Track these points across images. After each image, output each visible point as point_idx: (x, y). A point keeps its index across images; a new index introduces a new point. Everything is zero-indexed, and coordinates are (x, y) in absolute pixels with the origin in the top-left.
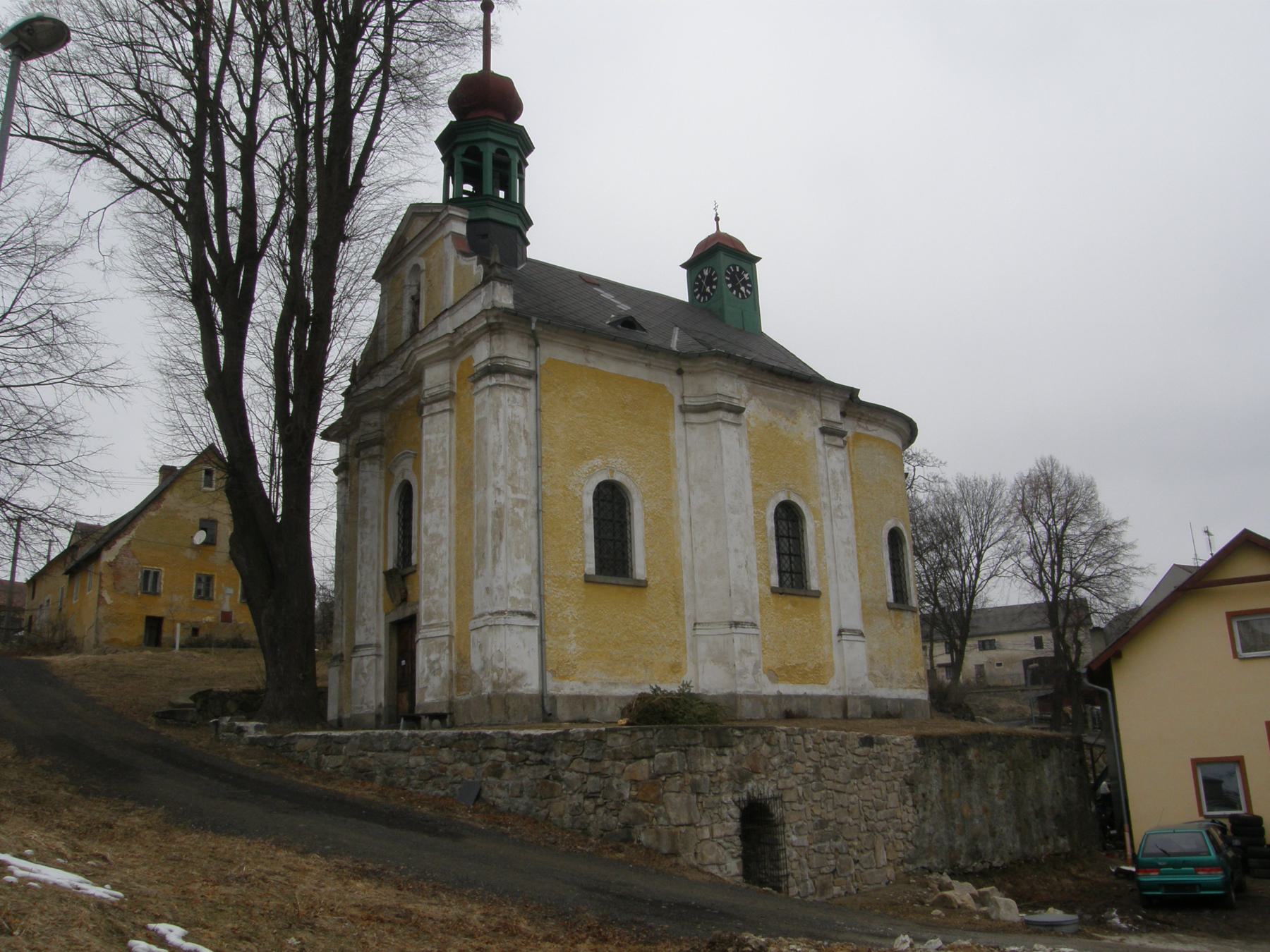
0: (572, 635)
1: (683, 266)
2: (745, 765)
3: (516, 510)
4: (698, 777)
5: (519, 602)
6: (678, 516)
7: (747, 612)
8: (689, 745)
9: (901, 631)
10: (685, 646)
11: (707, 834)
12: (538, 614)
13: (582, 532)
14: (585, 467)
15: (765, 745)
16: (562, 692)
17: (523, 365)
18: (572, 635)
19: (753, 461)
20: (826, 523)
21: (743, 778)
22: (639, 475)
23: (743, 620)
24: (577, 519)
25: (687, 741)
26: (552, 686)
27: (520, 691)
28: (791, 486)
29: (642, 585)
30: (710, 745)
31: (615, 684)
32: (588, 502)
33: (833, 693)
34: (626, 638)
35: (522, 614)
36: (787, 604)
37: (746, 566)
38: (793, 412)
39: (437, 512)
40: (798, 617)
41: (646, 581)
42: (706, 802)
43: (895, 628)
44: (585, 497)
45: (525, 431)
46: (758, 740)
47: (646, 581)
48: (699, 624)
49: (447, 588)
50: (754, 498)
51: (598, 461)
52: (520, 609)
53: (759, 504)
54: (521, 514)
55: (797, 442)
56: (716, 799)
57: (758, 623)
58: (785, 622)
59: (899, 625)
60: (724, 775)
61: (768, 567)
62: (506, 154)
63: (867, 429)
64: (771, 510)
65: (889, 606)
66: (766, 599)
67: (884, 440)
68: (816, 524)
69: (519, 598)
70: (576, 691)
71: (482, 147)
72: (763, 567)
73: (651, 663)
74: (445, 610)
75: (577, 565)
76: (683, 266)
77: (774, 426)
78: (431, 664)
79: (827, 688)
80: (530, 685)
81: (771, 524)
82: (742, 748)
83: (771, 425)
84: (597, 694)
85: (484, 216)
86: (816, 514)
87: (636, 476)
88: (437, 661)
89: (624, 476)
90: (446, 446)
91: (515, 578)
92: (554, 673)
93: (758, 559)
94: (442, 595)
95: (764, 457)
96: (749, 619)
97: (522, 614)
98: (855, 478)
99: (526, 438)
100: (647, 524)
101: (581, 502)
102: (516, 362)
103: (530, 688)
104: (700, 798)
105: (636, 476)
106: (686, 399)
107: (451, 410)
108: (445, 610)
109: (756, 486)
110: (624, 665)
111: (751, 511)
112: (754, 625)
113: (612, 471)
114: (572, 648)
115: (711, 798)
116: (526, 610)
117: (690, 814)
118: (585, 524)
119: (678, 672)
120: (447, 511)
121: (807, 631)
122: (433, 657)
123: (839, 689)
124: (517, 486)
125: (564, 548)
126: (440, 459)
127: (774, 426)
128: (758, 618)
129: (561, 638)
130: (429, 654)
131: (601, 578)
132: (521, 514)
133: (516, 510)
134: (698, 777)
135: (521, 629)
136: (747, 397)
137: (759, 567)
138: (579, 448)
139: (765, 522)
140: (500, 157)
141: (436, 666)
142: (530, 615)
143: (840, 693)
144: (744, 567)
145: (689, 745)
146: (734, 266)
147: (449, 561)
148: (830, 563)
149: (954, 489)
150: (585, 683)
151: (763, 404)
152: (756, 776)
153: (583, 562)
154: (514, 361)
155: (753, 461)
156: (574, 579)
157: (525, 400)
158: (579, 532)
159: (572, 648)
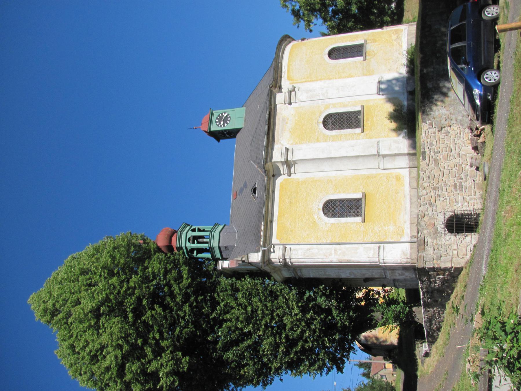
0: (386, 228)
2: (431, 231)
3: (338, 254)
4: (435, 257)
8: (424, 260)
9: (375, 52)
10: (388, 173)
11: (455, 252)
12: (378, 245)
13: (345, 223)
15: (424, 219)
16: (409, 233)
18: (386, 228)
20: (330, 101)
21: (436, 232)
22: (319, 196)
26: (407, 238)
27: (409, 253)
29: (364, 195)
32: (333, 220)
33: (406, 97)
35: (379, 252)
36: (367, 124)
41: (363, 193)
42: (444, 252)
43: (375, 56)
44: (331, 222)
46: (422, 223)
48: (378, 152)
49: (371, 271)
51: (315, 216)
53: (326, 139)
54: (340, 252)
56: (443, 247)
57: (377, 140)
59: (373, 53)
60: (435, 242)
64: (328, 132)
69: (373, 253)
71: (189, 249)
72: (353, 136)
73: (396, 190)
74: (379, 271)
76: (219, 141)
77: (291, 130)
78: (400, 275)
79: (404, 101)
80: (406, 248)
83: (290, 132)
84: (410, 217)
85: (218, 248)
86: (327, 107)
88: (399, 274)
91: (365, 254)
93: (349, 139)
96: (376, 145)
98: (308, 80)
100: (339, 192)
101: (333, 224)
103: (408, 248)
106: (285, 173)
107: (301, 270)
108: (379, 271)
109: (318, 141)
110: (397, 204)
112: (378, 143)
113: (319, 209)
114: (391, 228)
115: (443, 250)
116: (377, 250)
117: (448, 262)
118: (342, 222)
121: (379, 113)
122: (398, 275)
123: (404, 94)
126: (320, 273)
127: (291, 130)
128: (375, 140)
132: (340, 252)
135: (385, 252)
138: (311, 224)
142: (379, 248)
143: (406, 94)
145: (424, 260)
146: (216, 122)
148: (348, 99)
150: (405, 222)
153: (357, 223)
156: (364, 227)
157: (295, 250)
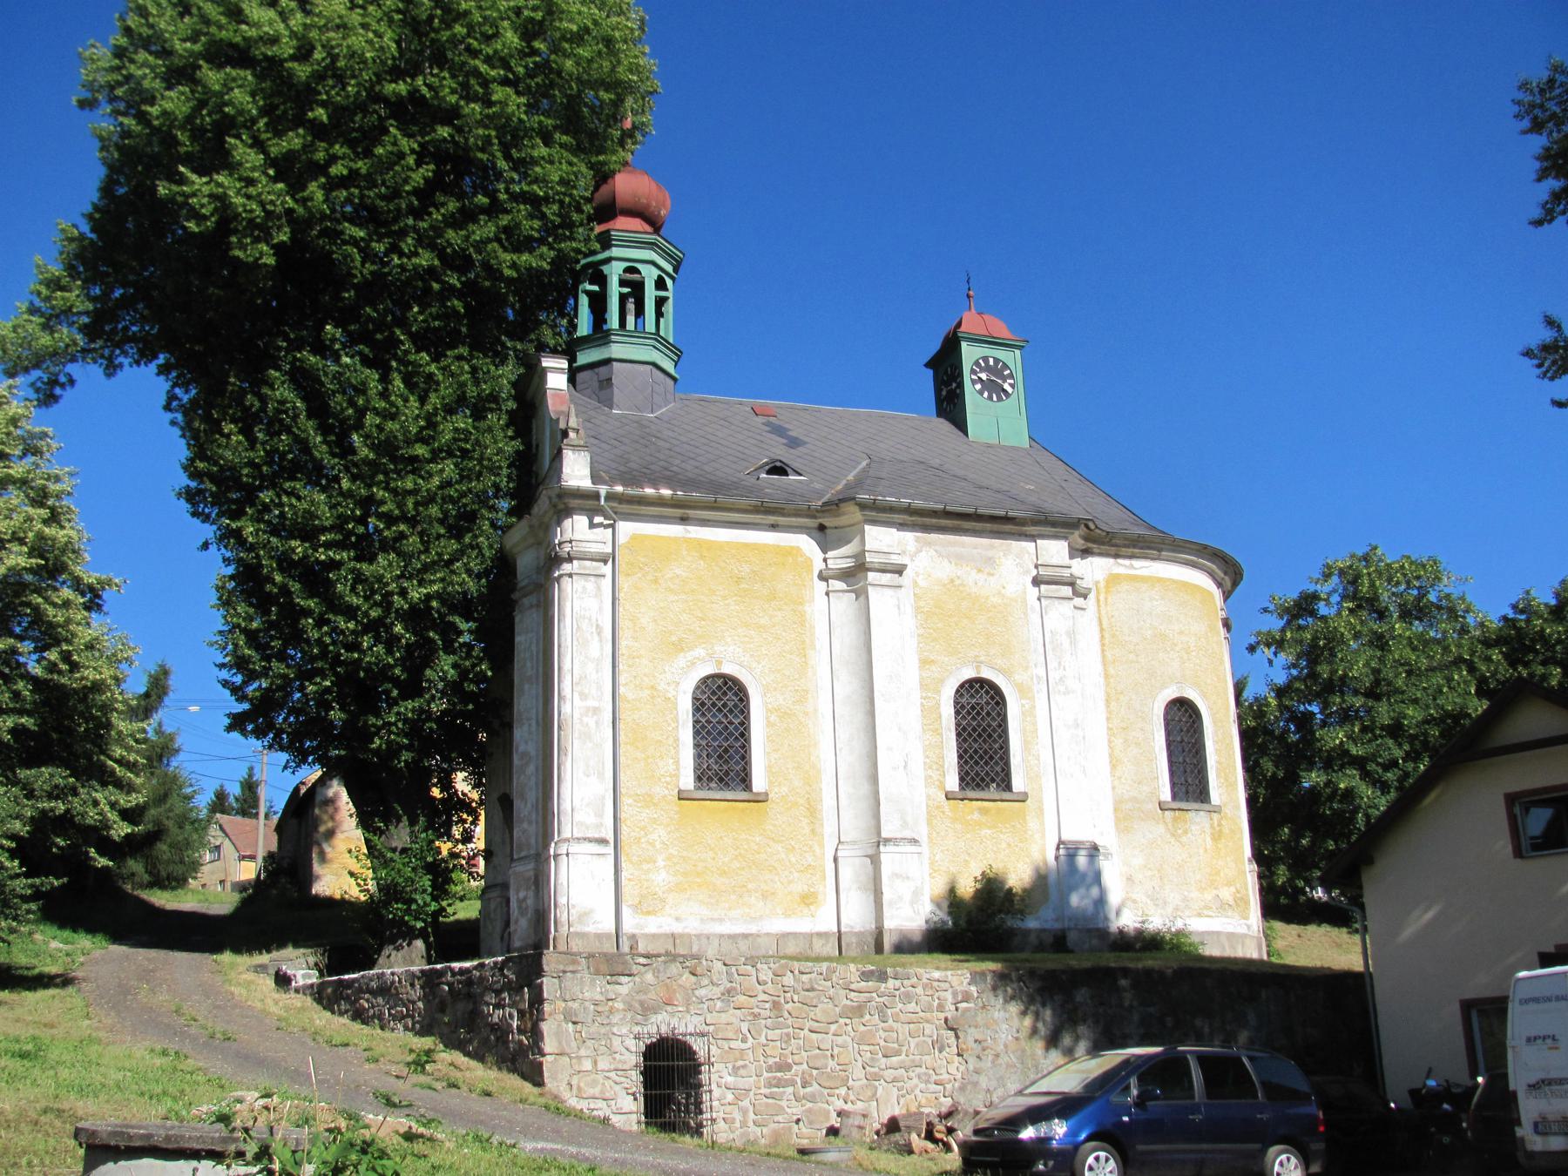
1: (927, 365)
2: (652, 995)
3: (585, 719)
4: (575, 1005)
5: (587, 828)
6: (816, 710)
7: (905, 824)
8: (564, 972)
9: (1184, 839)
12: (611, 838)
14: (681, 661)
16: (646, 931)
17: (595, 548)
18: (661, 863)
19: (921, 631)
21: (647, 1010)
23: (899, 836)
24: (669, 725)
25: (561, 967)
26: (630, 924)
27: (587, 929)
28: (982, 658)
29: (761, 799)
30: (597, 973)
31: (721, 920)
32: (685, 705)
34: (736, 864)
35: (590, 840)
36: (972, 810)
37: (905, 767)
38: (990, 561)
39: (525, 728)
40: (990, 828)
41: (766, 794)
45: (597, 626)
47: (766, 794)
50: (922, 679)
51: (700, 652)
52: (589, 835)
53: (929, 687)
54: (592, 724)
55: (995, 600)
57: (924, 840)
58: (969, 836)
61: (943, 766)
62: (639, 272)
63: (1132, 567)
65: (1162, 807)
66: (938, 807)
67: (1160, 580)
68: (1023, 706)
70: (666, 929)
71: (605, 269)
74: (533, 841)
75: (668, 779)
76: (927, 365)
78: (520, 902)
79: (1036, 919)
81: (948, 711)
82: (649, 977)
84: (694, 932)
87: (754, 665)
88: (525, 899)
89: (738, 667)
90: (534, 648)
92: (636, 908)
94: (530, 823)
95: (940, 625)
96: (908, 834)
97: (590, 840)
98: (1107, 636)
99: (599, 634)
100: (769, 724)
102: (588, 545)
103: (600, 926)
104: (579, 1027)
105: (754, 665)
108: (533, 841)
109: (925, 662)
111: (916, 695)
112: (914, 841)
114: (661, 878)
116: (597, 836)
119: (811, 904)
120: (534, 723)
121: (1004, 845)
122: (522, 895)
124: (586, 691)
125: (650, 760)
128: (922, 832)
129: (645, 867)
130: (518, 892)
131: (701, 794)
133: (585, 719)
134: (575, 1005)
136: (913, 549)
137: (927, 767)
138: (674, 638)
139: (939, 708)
140: (629, 276)
141: (524, 905)
142: (603, 841)
143: (1057, 926)
144: (902, 768)
147: (537, 784)
149: (1553, 602)
150: (677, 919)
151: (940, 555)
152: (669, 1008)
153: (676, 776)
154: (584, 544)
155: (921, 631)
157: (599, 588)
158: (671, 739)
159: (661, 878)
